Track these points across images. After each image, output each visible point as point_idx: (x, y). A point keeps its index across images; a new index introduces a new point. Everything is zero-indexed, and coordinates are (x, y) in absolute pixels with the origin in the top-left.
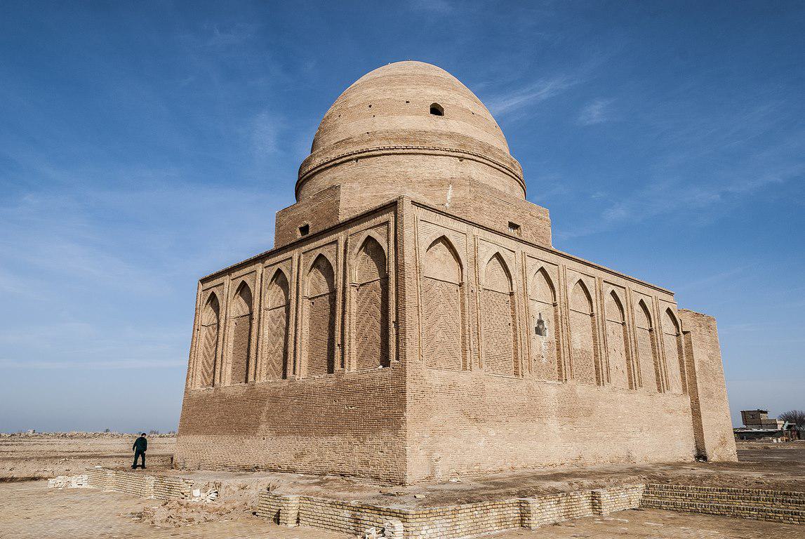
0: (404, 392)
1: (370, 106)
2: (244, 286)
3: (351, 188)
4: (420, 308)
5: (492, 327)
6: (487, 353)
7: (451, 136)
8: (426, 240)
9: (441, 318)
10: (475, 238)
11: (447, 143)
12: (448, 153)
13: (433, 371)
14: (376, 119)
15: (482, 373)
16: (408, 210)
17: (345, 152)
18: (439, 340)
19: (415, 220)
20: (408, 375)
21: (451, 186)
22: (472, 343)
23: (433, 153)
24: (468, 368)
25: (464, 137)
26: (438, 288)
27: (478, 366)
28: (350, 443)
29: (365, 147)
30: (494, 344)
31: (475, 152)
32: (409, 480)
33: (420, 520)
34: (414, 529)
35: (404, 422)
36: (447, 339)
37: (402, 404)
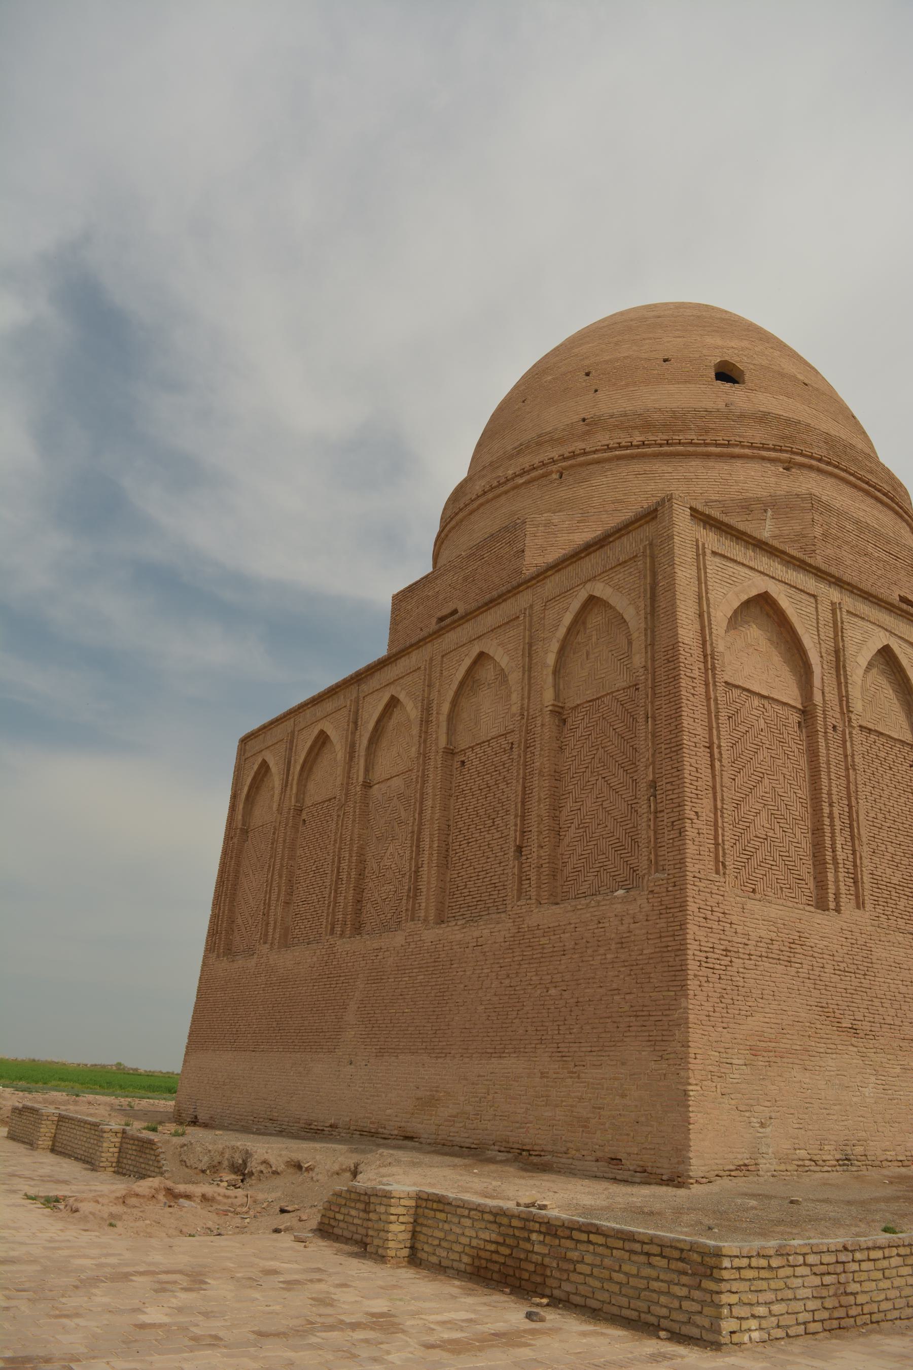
0: (681, 949)
1: (588, 374)
2: (324, 743)
3: (548, 524)
4: (716, 751)
5: (880, 816)
6: (876, 883)
7: (763, 418)
8: (721, 612)
9: (766, 781)
10: (834, 608)
11: (756, 434)
12: (757, 453)
13: (750, 904)
14: (600, 395)
15: (864, 917)
16: (685, 531)
17: (536, 461)
18: (761, 833)
19: (700, 553)
20: (692, 907)
21: (770, 513)
22: (839, 846)
23: (728, 452)
24: (832, 905)
25: (788, 421)
26: (755, 712)
27: (853, 902)
28: (543, 1075)
29: (579, 446)
30: (888, 856)
31: (816, 452)
32: (697, 1167)
33: (750, 1274)
34: (734, 1299)
35: (683, 1023)
36: (779, 832)
37: (677, 976)
